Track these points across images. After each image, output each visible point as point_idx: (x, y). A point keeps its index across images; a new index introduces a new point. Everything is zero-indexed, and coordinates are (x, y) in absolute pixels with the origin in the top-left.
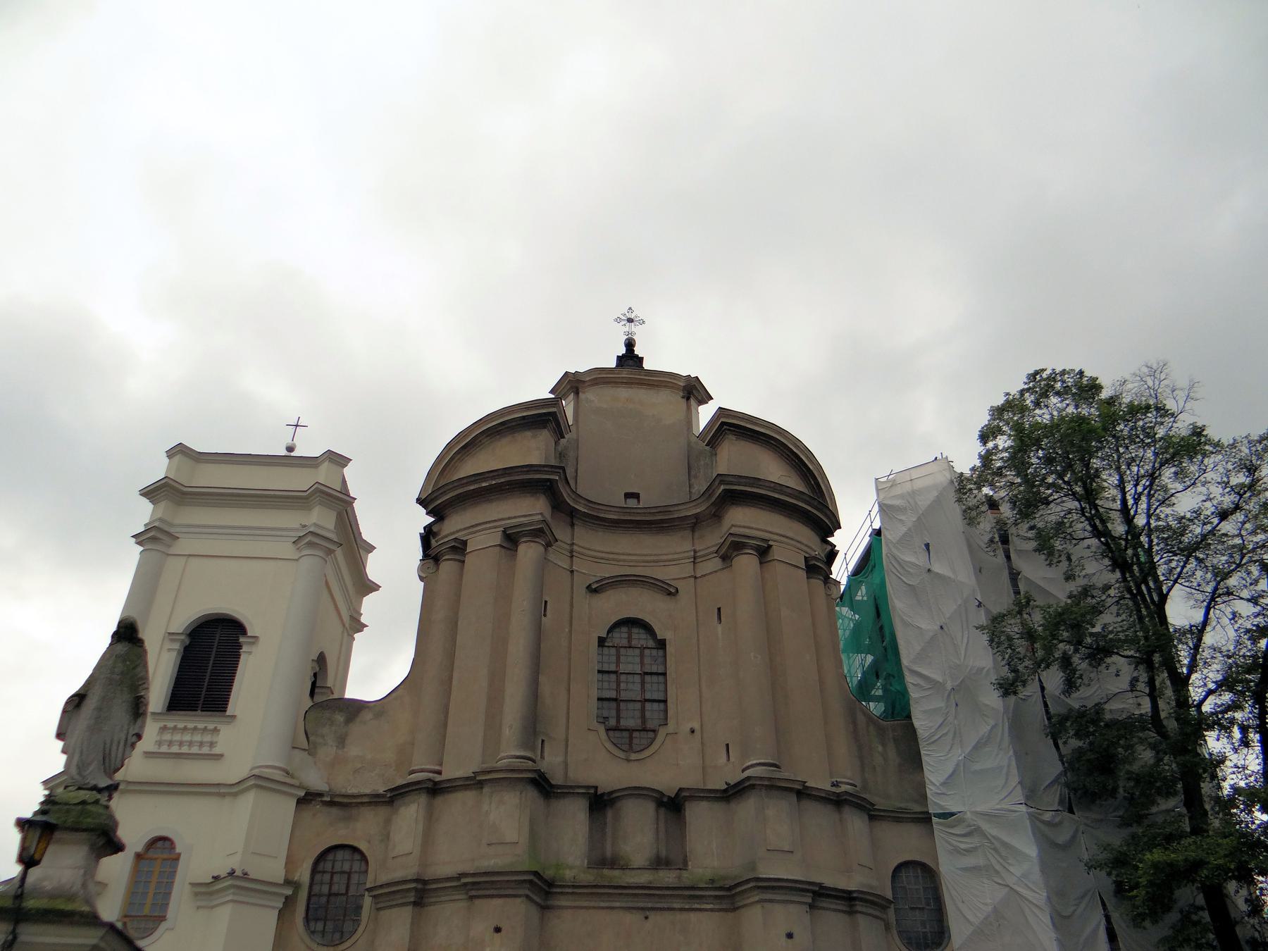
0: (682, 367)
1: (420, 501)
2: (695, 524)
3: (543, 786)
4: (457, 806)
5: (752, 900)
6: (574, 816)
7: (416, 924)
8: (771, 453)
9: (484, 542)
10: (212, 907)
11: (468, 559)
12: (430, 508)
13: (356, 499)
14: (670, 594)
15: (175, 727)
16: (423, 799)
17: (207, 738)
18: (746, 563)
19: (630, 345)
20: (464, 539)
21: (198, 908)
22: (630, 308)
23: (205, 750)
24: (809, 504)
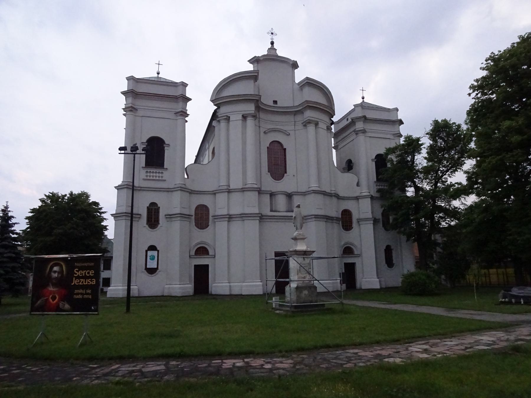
1: (212, 101)
2: (296, 113)
4: (235, 196)
5: (136, 220)
6: (266, 198)
7: (228, 225)
8: (319, 92)
9: (236, 118)
10: (172, 221)
11: (231, 123)
12: (215, 104)
13: (190, 99)
14: (288, 135)
15: (150, 171)
17: (160, 175)
18: (311, 128)
19: (272, 43)
20: (229, 116)
21: (168, 221)
22: (272, 29)
23: (160, 178)
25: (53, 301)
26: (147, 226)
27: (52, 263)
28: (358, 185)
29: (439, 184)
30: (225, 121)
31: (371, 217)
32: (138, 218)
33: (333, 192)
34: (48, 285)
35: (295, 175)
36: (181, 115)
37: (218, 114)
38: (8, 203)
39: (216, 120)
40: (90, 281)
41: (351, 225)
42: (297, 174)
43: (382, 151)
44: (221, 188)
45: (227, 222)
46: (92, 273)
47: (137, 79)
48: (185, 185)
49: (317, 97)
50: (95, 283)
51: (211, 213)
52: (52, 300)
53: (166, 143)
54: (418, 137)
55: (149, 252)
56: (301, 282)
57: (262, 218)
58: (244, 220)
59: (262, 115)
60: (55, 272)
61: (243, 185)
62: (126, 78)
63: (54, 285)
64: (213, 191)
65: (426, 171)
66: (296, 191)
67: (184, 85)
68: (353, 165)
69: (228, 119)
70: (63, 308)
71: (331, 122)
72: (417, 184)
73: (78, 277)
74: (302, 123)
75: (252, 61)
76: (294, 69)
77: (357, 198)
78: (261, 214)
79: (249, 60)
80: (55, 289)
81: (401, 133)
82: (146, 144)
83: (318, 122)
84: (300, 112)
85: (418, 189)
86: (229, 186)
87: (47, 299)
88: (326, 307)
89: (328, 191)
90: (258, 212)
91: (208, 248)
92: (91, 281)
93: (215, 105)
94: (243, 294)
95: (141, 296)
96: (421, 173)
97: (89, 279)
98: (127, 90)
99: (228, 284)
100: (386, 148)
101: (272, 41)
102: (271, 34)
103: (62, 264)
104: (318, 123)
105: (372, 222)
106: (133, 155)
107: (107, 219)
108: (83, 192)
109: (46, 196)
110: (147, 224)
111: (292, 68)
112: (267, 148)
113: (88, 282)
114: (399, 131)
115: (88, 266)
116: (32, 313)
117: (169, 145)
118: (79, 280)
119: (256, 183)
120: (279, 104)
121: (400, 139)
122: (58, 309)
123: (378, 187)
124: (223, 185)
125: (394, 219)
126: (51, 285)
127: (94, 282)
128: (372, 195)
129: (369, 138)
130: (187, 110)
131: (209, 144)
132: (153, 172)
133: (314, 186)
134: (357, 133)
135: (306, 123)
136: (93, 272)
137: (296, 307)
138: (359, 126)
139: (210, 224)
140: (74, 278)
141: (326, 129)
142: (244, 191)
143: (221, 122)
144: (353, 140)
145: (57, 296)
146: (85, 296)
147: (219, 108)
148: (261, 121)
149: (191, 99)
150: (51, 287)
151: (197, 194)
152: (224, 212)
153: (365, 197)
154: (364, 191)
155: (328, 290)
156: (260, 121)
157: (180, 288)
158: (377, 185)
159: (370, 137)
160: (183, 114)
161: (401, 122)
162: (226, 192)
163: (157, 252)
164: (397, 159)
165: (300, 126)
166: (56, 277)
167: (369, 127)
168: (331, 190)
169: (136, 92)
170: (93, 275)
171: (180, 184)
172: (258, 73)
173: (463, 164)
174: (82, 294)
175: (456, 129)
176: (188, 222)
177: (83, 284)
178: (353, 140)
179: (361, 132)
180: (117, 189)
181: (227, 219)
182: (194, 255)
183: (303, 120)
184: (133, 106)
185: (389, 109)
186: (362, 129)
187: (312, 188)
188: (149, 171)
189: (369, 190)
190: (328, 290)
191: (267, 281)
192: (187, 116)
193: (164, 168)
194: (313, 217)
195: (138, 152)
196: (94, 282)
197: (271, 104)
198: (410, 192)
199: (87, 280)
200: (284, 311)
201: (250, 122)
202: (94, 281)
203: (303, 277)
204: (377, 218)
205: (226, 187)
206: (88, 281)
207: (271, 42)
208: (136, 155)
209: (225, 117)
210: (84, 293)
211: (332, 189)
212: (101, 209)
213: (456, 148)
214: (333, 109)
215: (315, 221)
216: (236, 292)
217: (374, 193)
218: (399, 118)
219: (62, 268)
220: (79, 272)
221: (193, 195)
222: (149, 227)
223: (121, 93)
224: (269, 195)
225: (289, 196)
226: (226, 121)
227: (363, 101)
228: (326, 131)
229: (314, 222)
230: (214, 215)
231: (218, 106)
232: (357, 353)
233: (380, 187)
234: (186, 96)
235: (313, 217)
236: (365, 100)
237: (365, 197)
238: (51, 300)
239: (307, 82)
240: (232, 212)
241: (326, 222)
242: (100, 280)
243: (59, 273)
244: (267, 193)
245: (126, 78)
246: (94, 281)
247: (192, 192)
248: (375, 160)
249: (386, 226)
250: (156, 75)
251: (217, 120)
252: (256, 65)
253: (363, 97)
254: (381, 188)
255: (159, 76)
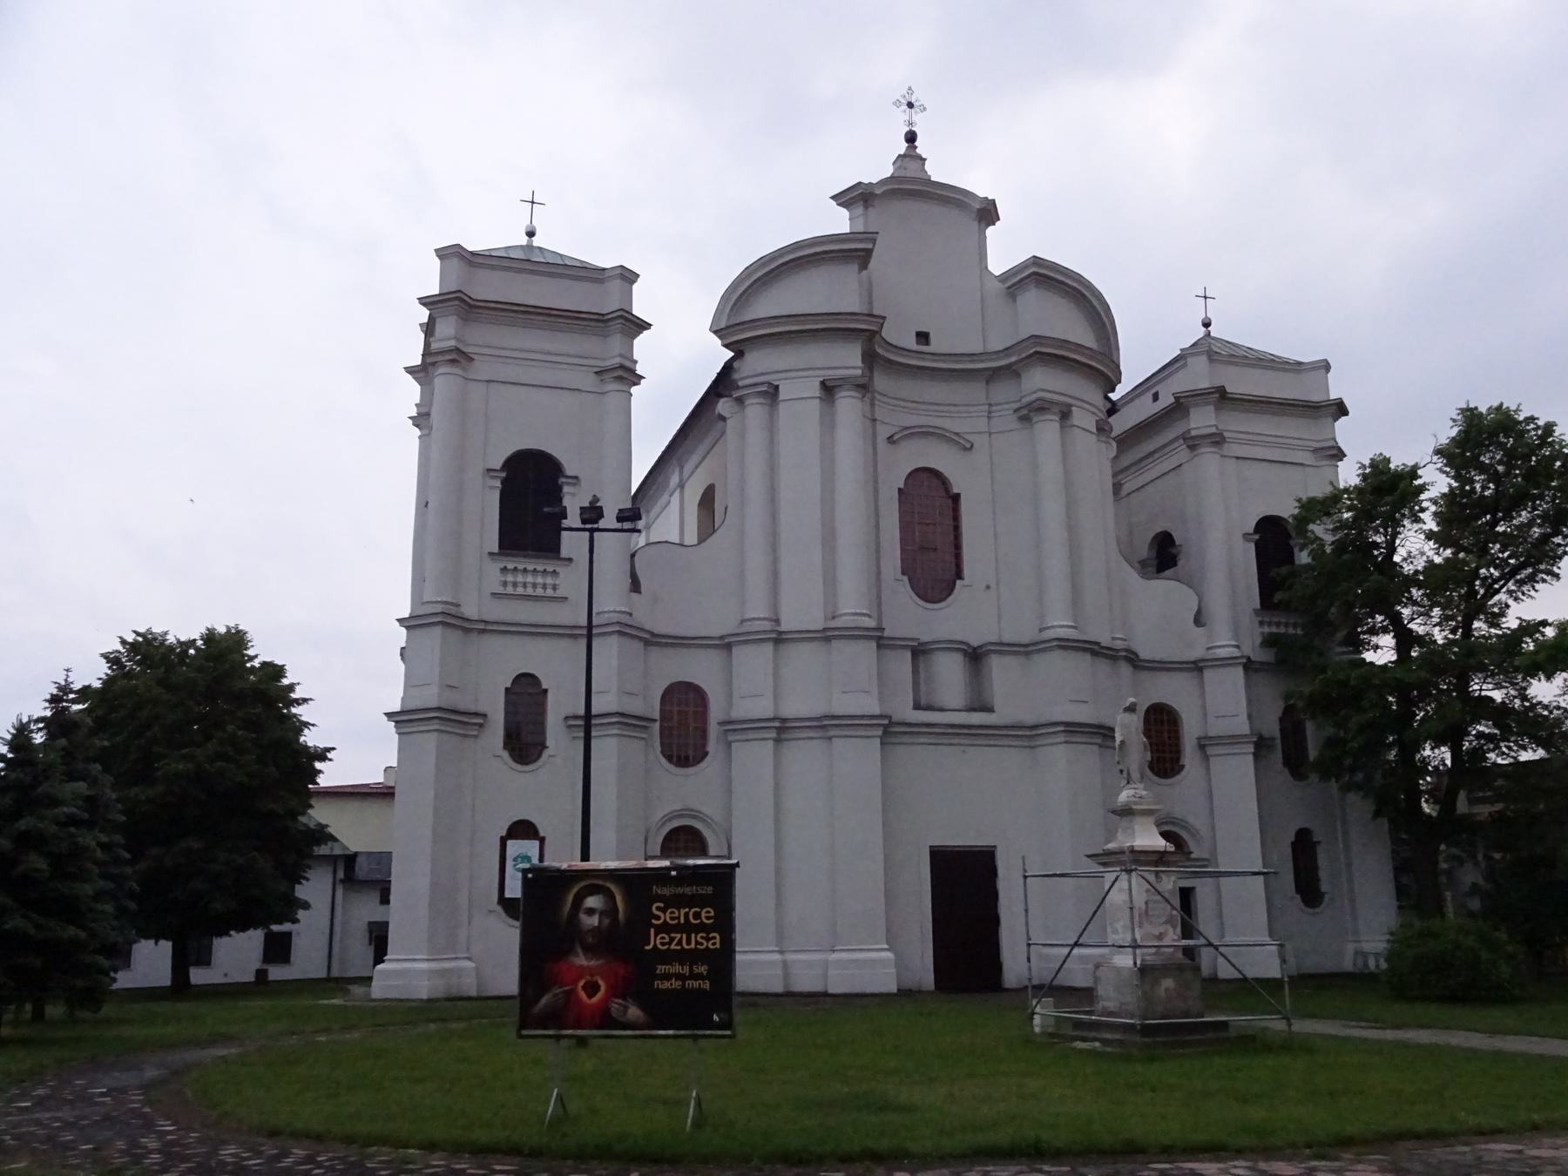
0: (979, 185)
2: (992, 376)
3: (882, 641)
4: (802, 657)
6: (902, 663)
7: (884, 759)
9: (800, 392)
13: (646, 326)
14: (965, 449)
16: (768, 648)
17: (549, 580)
18: (1048, 429)
19: (911, 138)
20: (776, 383)
21: (574, 738)
22: (910, 89)
23: (549, 592)
24: (1099, 361)
25: (590, 996)
26: (505, 754)
27: (583, 884)
28: (1199, 620)
29: (1476, 624)
30: (761, 400)
31: (1246, 730)
32: (477, 727)
33: (1119, 644)
34: (570, 951)
35: (993, 585)
36: (620, 379)
37: (736, 376)
38: (69, 674)
39: (731, 396)
40: (702, 937)
41: (1178, 759)
42: (998, 583)
43: (1286, 509)
44: (748, 627)
45: (771, 744)
46: (706, 915)
47: (472, 253)
48: (631, 614)
49: (1069, 327)
50: (718, 946)
51: (715, 713)
52: (586, 993)
53: (569, 472)
54: (1411, 463)
55: (509, 843)
56: (1153, 950)
57: (889, 730)
58: (830, 738)
59: (881, 382)
60: (591, 912)
61: (826, 619)
62: (436, 251)
63: (589, 950)
64: (722, 637)
65: (1436, 580)
66: (994, 639)
67: (627, 277)
68: (1179, 553)
69: (772, 394)
70: (621, 1019)
71: (1109, 405)
72: (1406, 622)
73: (665, 928)
74: (1015, 411)
75: (845, 199)
76: (983, 224)
77: (1197, 667)
78: (890, 717)
79: (833, 194)
80: (593, 963)
81: (1341, 444)
82: (504, 475)
83: (1071, 406)
84: (1011, 372)
85: (1405, 639)
86: (777, 621)
87: (571, 994)
88: (1232, 1033)
89: (1105, 640)
90: (877, 711)
91: (706, 833)
92: (708, 939)
93: (726, 346)
94: (831, 991)
95: (484, 995)
96: (1420, 585)
97: (699, 932)
98: (437, 293)
99: (777, 957)
100: (1299, 500)
101: (910, 130)
102: (906, 102)
103: (613, 887)
104: (1070, 411)
105: (1251, 749)
106: (587, 534)
107: (313, 725)
108: (233, 631)
109: (123, 642)
110: (505, 748)
111: (979, 222)
112: (897, 490)
113: (697, 943)
114: (1334, 439)
115: (693, 895)
116: (524, 1032)
117: (576, 478)
118: (668, 934)
119: (868, 612)
120: (936, 345)
121: (1338, 466)
122: (605, 1020)
123: (1266, 629)
124: (755, 616)
125: (1330, 743)
126: (580, 950)
127: (716, 942)
128: (1249, 658)
129: (1234, 460)
130: (636, 362)
131: (681, 473)
132: (525, 570)
133: (1061, 623)
134: (1193, 443)
135: (1030, 411)
136: (712, 914)
137: (1147, 1030)
138: (1202, 420)
139: (712, 746)
140: (652, 930)
141: (1094, 430)
142: (828, 639)
143: (747, 402)
144: (1180, 465)
145: (601, 982)
146: (691, 984)
147: (739, 354)
148: (879, 400)
149: (651, 325)
150: (581, 954)
151: (673, 645)
152: (762, 708)
153: (1225, 662)
154: (1223, 642)
155: (1240, 972)
156: (876, 402)
157: (432, 972)
158: (1261, 623)
159: (1237, 458)
160: (625, 375)
161: (1340, 409)
162: (769, 639)
163: (537, 843)
164: (1337, 537)
165: (1005, 420)
166: (595, 927)
167: (1234, 423)
168: (1114, 639)
169: (474, 300)
170: (711, 921)
171: (615, 612)
172: (874, 241)
173: (1560, 558)
174: (679, 977)
175: (1539, 437)
176: (643, 742)
177: (682, 947)
178: (1180, 465)
179: (1209, 440)
180: (407, 627)
181: (774, 735)
182: (659, 854)
183: (1020, 400)
184: (460, 346)
185: (1300, 363)
186: (1214, 430)
187: (1052, 631)
188: (510, 566)
189: (1236, 641)
190: (1240, 972)
191: (1029, 945)
192: (636, 381)
193: (559, 558)
194: (1062, 728)
195: (602, 524)
196: (716, 942)
197: (911, 343)
198: (1382, 651)
199: (693, 935)
200: (1104, 1042)
201: (848, 405)
202: (714, 938)
203: (1157, 934)
204: (1266, 734)
205: (767, 626)
206: (696, 937)
207: (906, 134)
208: (596, 534)
209: (764, 388)
210: (687, 974)
211: (1117, 636)
212: (291, 687)
213: (1534, 502)
214: (1115, 359)
215: (1066, 742)
216: (806, 982)
217: (1251, 647)
218: (1333, 396)
219: (613, 898)
220: (668, 914)
221: (655, 651)
222: (511, 755)
223: (422, 304)
224: (909, 655)
225: (975, 657)
226: (768, 401)
227: (1208, 334)
228: (1094, 437)
229: (1062, 747)
230: (727, 719)
231: (739, 350)
232: (1520, 1152)
233: (1274, 630)
234: (634, 313)
235: (1062, 728)
236: (1215, 331)
237: (1225, 662)
238: (583, 995)
239: (1034, 273)
240: (792, 709)
241: (1100, 746)
242: (733, 937)
243: (602, 913)
244: (903, 647)
245: (436, 251)
246: (714, 938)
247: (653, 640)
248: (1257, 537)
249: (1295, 763)
250: (524, 240)
251: (734, 396)
252: (859, 210)
253: (1207, 321)
254: (1275, 633)
255: (535, 244)
